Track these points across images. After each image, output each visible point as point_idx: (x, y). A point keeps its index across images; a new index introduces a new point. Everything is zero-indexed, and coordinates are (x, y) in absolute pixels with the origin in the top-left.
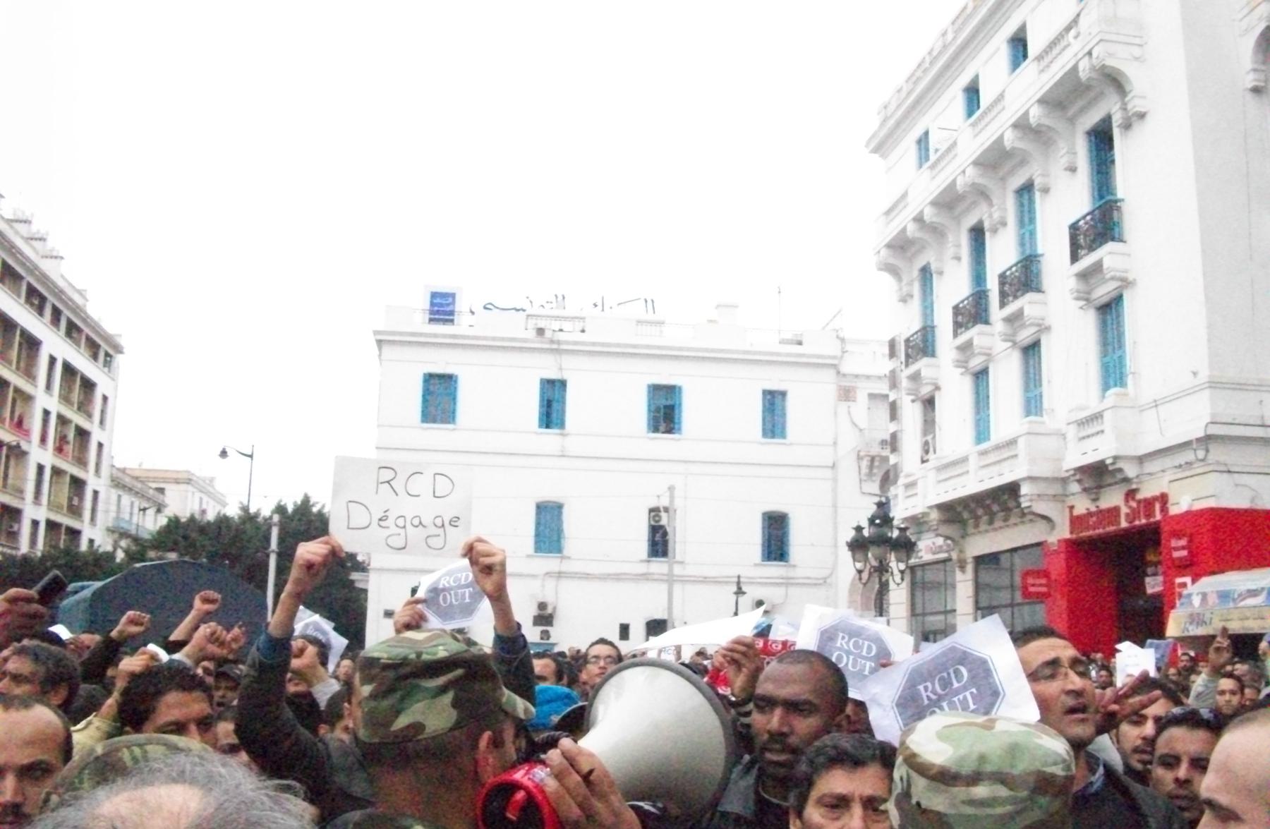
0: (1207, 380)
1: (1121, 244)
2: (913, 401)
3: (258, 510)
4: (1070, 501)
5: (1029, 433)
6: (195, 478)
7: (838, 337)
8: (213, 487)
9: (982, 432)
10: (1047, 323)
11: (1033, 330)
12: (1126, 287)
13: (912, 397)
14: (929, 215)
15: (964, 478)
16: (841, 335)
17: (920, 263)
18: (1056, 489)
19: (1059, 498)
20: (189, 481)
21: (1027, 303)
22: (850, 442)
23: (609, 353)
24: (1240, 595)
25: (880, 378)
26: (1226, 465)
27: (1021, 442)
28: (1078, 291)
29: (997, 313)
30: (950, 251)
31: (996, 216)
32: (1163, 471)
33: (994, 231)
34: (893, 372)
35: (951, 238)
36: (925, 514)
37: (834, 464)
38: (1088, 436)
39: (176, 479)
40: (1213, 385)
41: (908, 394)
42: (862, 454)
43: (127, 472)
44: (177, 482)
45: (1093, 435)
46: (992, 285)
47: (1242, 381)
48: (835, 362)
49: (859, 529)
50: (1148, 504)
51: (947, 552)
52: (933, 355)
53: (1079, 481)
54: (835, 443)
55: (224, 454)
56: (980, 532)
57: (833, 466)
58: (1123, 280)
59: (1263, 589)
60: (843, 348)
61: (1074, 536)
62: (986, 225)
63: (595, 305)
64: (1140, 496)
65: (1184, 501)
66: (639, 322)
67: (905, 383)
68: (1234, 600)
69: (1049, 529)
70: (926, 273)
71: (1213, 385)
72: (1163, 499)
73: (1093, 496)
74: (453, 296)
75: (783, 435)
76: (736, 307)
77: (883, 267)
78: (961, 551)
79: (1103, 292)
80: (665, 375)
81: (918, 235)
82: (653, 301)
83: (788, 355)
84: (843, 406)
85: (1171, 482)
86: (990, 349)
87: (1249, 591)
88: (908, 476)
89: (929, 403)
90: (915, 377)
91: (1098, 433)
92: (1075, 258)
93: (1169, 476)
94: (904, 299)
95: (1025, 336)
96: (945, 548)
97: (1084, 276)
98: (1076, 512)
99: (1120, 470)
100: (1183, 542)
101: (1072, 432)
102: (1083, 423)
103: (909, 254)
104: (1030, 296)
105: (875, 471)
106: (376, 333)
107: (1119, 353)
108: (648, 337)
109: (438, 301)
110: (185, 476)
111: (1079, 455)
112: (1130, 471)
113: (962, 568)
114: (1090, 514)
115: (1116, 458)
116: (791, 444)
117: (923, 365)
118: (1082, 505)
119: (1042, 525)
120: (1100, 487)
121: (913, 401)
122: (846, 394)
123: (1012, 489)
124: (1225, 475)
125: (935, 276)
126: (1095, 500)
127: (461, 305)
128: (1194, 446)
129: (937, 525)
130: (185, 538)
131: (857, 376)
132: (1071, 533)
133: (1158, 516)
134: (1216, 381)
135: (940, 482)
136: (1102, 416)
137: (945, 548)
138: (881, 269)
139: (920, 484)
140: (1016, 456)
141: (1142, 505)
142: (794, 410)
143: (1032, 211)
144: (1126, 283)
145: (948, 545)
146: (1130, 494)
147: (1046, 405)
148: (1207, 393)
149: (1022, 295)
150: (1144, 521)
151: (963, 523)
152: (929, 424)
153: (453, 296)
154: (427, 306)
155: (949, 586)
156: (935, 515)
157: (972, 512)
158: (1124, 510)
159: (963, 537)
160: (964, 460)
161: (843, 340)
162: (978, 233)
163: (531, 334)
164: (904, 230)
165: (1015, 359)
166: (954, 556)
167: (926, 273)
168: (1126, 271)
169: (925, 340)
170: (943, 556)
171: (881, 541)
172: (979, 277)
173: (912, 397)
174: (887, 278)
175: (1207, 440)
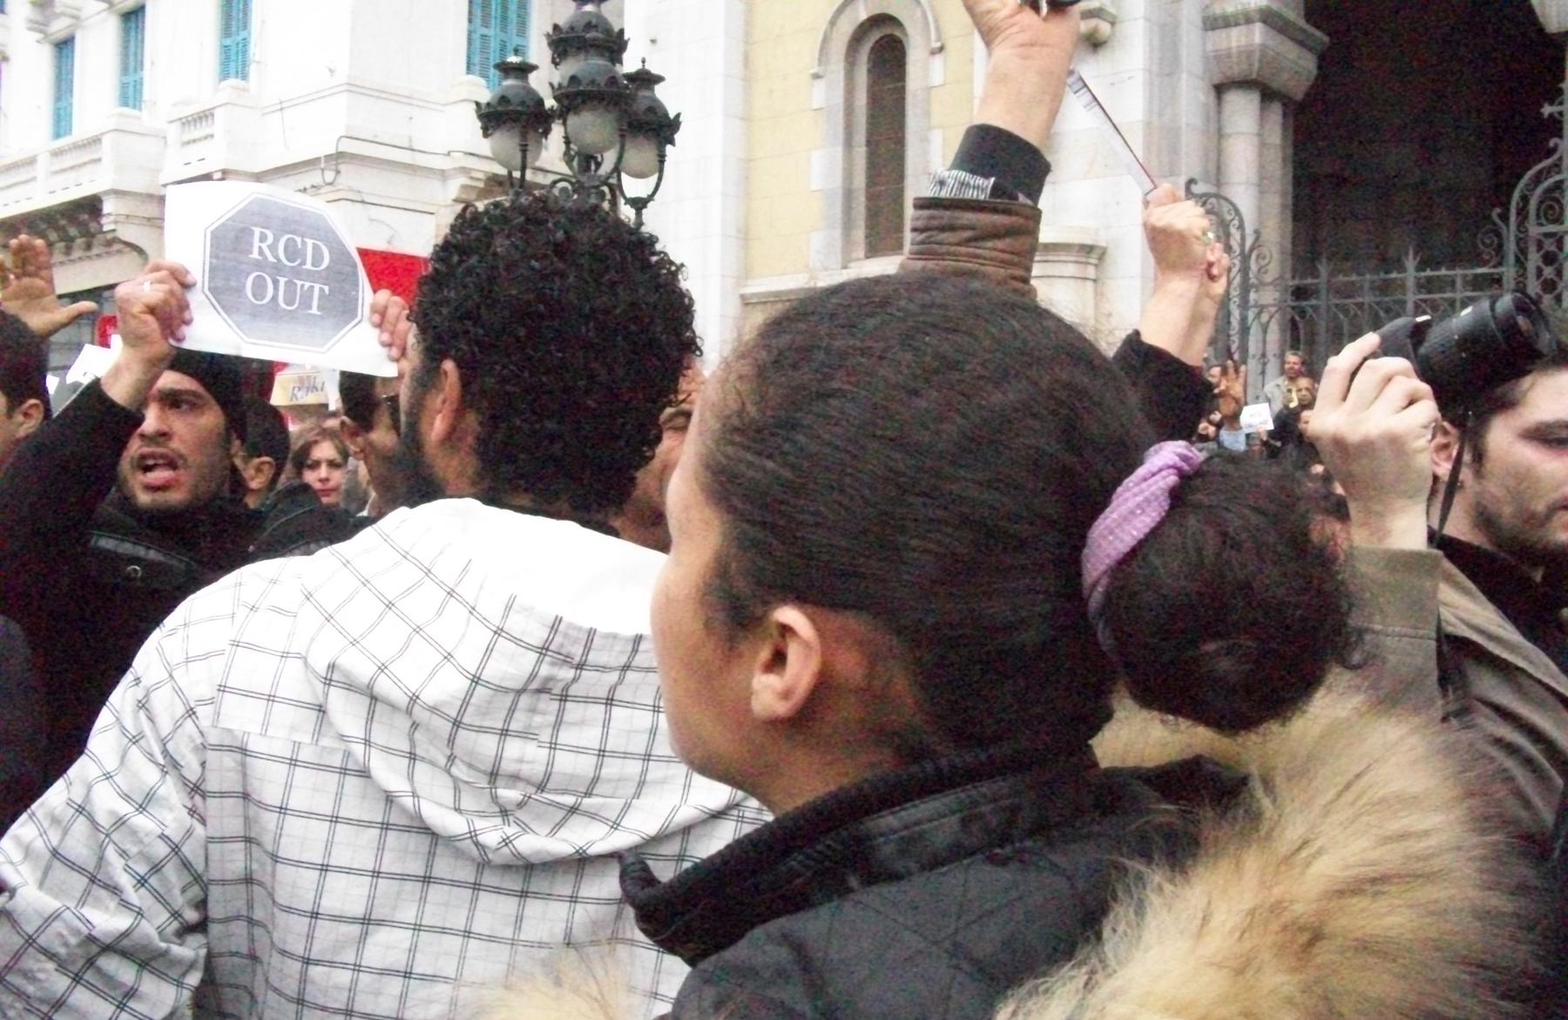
0: (344, 80)
9: (61, 122)
15: (28, 187)
27: (106, 140)
38: (194, 141)
45: (200, 140)
101: (174, 132)
102: (189, 122)
107: (243, 34)
123: (91, 207)
124: (359, 205)
136: (212, 115)
140: (99, 160)
147: (146, 95)
160: (31, 161)
175: (339, 157)
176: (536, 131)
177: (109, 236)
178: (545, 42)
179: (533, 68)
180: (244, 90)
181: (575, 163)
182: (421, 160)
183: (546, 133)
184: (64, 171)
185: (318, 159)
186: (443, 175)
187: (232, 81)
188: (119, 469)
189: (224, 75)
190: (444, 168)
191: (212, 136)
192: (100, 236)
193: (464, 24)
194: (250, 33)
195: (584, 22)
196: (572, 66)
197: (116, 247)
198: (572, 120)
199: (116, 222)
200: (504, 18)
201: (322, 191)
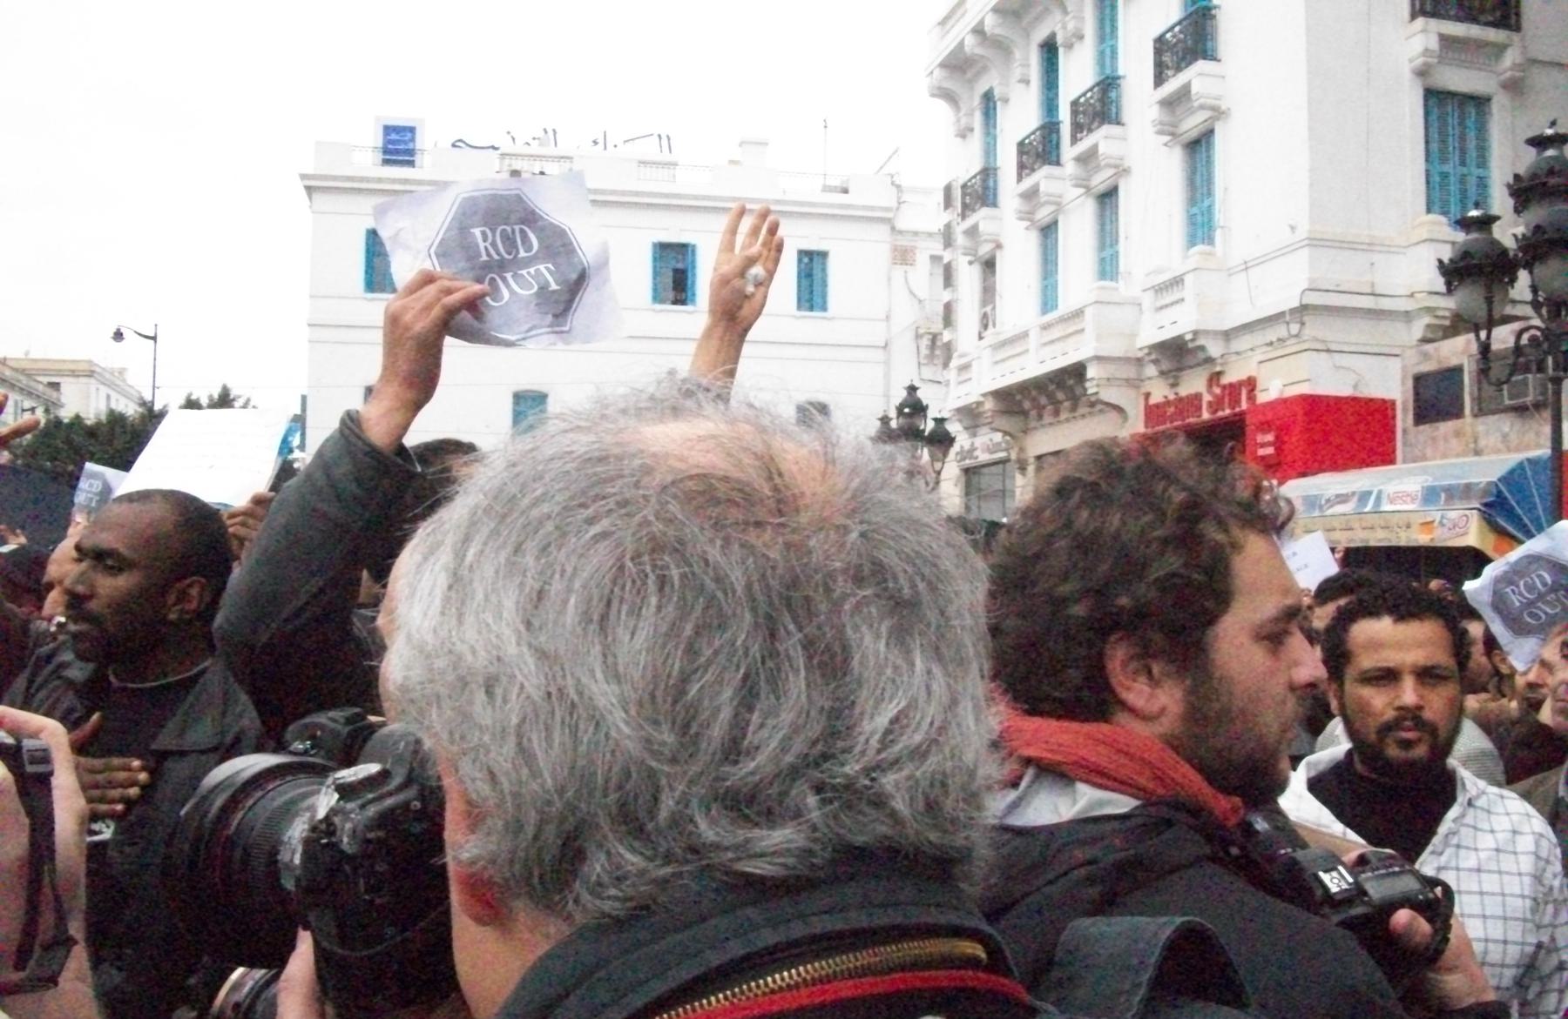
0: (1305, 235)
1: (1213, 63)
2: (971, 263)
3: (165, 407)
4: (1147, 387)
5: (1096, 302)
6: (98, 369)
7: (893, 183)
8: (124, 381)
9: (1048, 300)
10: (1126, 165)
11: (1111, 172)
12: (1218, 119)
13: (969, 258)
14: (990, 23)
16: (897, 182)
17: (982, 87)
18: (1130, 372)
19: (1133, 383)
20: (91, 374)
21: (1102, 138)
22: (906, 316)
23: (706, 209)
24: (1328, 501)
25: (930, 235)
26: (1324, 341)
27: (1089, 312)
28: (1161, 123)
29: (1068, 152)
30: (1017, 72)
31: (1071, 26)
32: (1252, 350)
33: (1069, 46)
34: (948, 226)
35: (1018, 54)
36: (979, 404)
37: (886, 344)
38: (1167, 306)
39: (73, 371)
40: (1315, 242)
41: (965, 254)
42: (921, 331)
43: (8, 363)
44: (74, 374)
46: (1064, 114)
47: (1350, 239)
48: (890, 215)
49: (885, 420)
50: (1233, 390)
51: (1006, 450)
52: (995, 205)
53: (1155, 362)
54: (888, 318)
55: (118, 336)
56: (1043, 426)
57: (885, 347)
58: (1214, 109)
59: (1354, 493)
60: (899, 198)
61: (1150, 431)
62: (1060, 40)
63: (595, 143)
64: (1226, 380)
65: (1272, 389)
66: (643, 163)
67: (960, 239)
68: (1321, 507)
69: (1120, 421)
70: (989, 100)
71: (1315, 242)
72: (1251, 384)
73: (1171, 381)
74: (412, 130)
75: (824, 308)
76: (767, 144)
77: (935, 92)
78: (1022, 450)
79: (1192, 124)
80: (674, 233)
81: (979, 51)
82: (668, 137)
83: (831, 206)
84: (899, 271)
85: (1261, 362)
86: (1060, 197)
87: (1338, 496)
88: (961, 356)
89: (989, 265)
90: (972, 232)
91: (1177, 302)
92: (1159, 80)
93: (1258, 356)
94: (964, 133)
95: (1100, 181)
96: (1004, 445)
97: (1169, 104)
98: (1153, 400)
99: (1202, 348)
100: (1270, 437)
101: (1148, 300)
102: (1161, 289)
103: (969, 75)
104: (1106, 129)
105: (938, 352)
106: (304, 177)
108: (655, 182)
109: (394, 136)
110: (86, 367)
111: (1155, 329)
112: (1214, 349)
113: (1023, 469)
114: (1168, 403)
115: (1196, 333)
116: (833, 318)
117: (981, 216)
118: (1160, 392)
119: (1113, 415)
120: (1180, 369)
121: (971, 263)
122: (903, 256)
123: (1077, 372)
124: (1324, 355)
125: (999, 104)
126: (1174, 385)
127: (423, 141)
128: (1288, 318)
129: (992, 417)
130: (69, 442)
131: (916, 233)
132: (1146, 427)
133: (1244, 405)
134: (1319, 236)
135: (996, 363)
136: (1182, 280)
137: (1004, 445)
138: (933, 95)
139: (975, 364)
140: (1083, 330)
141: (1227, 392)
142: (837, 275)
143: (1113, 20)
144: (1218, 113)
145: (1007, 442)
146: (1215, 378)
147: (1122, 268)
148: (1306, 251)
149: (1098, 127)
150: (1228, 412)
151: (1025, 414)
152: (988, 292)
153: (412, 130)
154: (380, 144)
155: (1007, 494)
156: (989, 405)
157: (1051, 398)
158: (1207, 398)
159: (1025, 432)
160: (1025, 335)
161: (898, 187)
162: (1050, 50)
163: (505, 175)
164: (961, 44)
165: (1089, 208)
166: (1013, 456)
167: (989, 100)
168: (1218, 98)
169: (985, 188)
170: (1002, 455)
171: (911, 434)
172: (1050, 104)
173: (969, 258)
174: (942, 106)
175: (1304, 309)
176: (1501, 281)
177: (1093, 399)
178: (1506, 192)
179: (1496, 218)
180: (1210, 254)
181: (1544, 311)
182: (1386, 304)
183: (1513, 280)
184: (1052, 342)
185: (1282, 314)
186: (1407, 316)
187: (1200, 248)
188: (1210, 633)
189: (1192, 241)
190: (1409, 309)
191: (1183, 300)
192: (1084, 399)
193: (1420, 165)
194: (1214, 201)
195: (1545, 166)
196: (1538, 213)
197: (1099, 407)
198: (1539, 269)
199: (1098, 386)
200: (1463, 151)
201: (1288, 343)
